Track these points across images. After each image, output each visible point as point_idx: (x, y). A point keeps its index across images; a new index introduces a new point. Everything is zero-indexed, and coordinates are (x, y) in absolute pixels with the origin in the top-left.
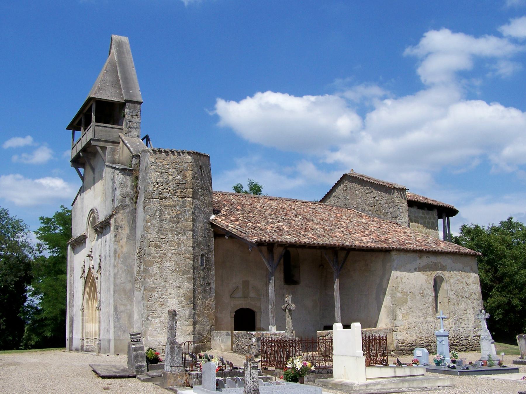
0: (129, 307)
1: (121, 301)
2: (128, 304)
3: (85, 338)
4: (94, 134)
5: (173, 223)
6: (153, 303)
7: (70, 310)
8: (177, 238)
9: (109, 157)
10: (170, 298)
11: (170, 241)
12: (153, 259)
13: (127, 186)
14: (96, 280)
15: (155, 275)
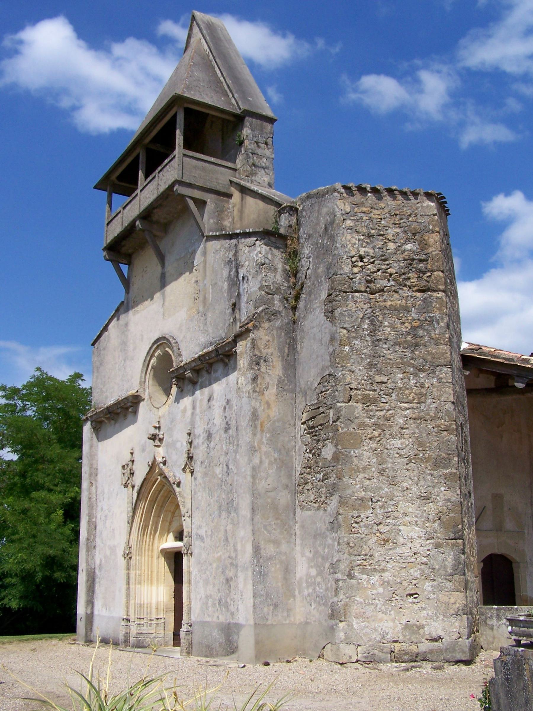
0: (284, 547)
1: (269, 532)
2: (283, 541)
3: (132, 617)
4: (181, 172)
5: (404, 348)
6: (363, 536)
7: (88, 555)
8: (415, 381)
9: (212, 221)
10: (405, 525)
11: (400, 389)
12: (360, 431)
13: (276, 269)
14: (177, 489)
15: (365, 469)
